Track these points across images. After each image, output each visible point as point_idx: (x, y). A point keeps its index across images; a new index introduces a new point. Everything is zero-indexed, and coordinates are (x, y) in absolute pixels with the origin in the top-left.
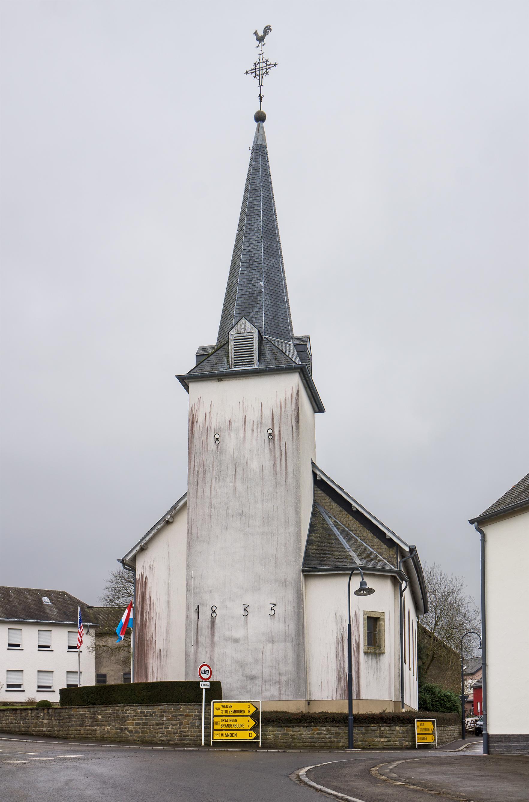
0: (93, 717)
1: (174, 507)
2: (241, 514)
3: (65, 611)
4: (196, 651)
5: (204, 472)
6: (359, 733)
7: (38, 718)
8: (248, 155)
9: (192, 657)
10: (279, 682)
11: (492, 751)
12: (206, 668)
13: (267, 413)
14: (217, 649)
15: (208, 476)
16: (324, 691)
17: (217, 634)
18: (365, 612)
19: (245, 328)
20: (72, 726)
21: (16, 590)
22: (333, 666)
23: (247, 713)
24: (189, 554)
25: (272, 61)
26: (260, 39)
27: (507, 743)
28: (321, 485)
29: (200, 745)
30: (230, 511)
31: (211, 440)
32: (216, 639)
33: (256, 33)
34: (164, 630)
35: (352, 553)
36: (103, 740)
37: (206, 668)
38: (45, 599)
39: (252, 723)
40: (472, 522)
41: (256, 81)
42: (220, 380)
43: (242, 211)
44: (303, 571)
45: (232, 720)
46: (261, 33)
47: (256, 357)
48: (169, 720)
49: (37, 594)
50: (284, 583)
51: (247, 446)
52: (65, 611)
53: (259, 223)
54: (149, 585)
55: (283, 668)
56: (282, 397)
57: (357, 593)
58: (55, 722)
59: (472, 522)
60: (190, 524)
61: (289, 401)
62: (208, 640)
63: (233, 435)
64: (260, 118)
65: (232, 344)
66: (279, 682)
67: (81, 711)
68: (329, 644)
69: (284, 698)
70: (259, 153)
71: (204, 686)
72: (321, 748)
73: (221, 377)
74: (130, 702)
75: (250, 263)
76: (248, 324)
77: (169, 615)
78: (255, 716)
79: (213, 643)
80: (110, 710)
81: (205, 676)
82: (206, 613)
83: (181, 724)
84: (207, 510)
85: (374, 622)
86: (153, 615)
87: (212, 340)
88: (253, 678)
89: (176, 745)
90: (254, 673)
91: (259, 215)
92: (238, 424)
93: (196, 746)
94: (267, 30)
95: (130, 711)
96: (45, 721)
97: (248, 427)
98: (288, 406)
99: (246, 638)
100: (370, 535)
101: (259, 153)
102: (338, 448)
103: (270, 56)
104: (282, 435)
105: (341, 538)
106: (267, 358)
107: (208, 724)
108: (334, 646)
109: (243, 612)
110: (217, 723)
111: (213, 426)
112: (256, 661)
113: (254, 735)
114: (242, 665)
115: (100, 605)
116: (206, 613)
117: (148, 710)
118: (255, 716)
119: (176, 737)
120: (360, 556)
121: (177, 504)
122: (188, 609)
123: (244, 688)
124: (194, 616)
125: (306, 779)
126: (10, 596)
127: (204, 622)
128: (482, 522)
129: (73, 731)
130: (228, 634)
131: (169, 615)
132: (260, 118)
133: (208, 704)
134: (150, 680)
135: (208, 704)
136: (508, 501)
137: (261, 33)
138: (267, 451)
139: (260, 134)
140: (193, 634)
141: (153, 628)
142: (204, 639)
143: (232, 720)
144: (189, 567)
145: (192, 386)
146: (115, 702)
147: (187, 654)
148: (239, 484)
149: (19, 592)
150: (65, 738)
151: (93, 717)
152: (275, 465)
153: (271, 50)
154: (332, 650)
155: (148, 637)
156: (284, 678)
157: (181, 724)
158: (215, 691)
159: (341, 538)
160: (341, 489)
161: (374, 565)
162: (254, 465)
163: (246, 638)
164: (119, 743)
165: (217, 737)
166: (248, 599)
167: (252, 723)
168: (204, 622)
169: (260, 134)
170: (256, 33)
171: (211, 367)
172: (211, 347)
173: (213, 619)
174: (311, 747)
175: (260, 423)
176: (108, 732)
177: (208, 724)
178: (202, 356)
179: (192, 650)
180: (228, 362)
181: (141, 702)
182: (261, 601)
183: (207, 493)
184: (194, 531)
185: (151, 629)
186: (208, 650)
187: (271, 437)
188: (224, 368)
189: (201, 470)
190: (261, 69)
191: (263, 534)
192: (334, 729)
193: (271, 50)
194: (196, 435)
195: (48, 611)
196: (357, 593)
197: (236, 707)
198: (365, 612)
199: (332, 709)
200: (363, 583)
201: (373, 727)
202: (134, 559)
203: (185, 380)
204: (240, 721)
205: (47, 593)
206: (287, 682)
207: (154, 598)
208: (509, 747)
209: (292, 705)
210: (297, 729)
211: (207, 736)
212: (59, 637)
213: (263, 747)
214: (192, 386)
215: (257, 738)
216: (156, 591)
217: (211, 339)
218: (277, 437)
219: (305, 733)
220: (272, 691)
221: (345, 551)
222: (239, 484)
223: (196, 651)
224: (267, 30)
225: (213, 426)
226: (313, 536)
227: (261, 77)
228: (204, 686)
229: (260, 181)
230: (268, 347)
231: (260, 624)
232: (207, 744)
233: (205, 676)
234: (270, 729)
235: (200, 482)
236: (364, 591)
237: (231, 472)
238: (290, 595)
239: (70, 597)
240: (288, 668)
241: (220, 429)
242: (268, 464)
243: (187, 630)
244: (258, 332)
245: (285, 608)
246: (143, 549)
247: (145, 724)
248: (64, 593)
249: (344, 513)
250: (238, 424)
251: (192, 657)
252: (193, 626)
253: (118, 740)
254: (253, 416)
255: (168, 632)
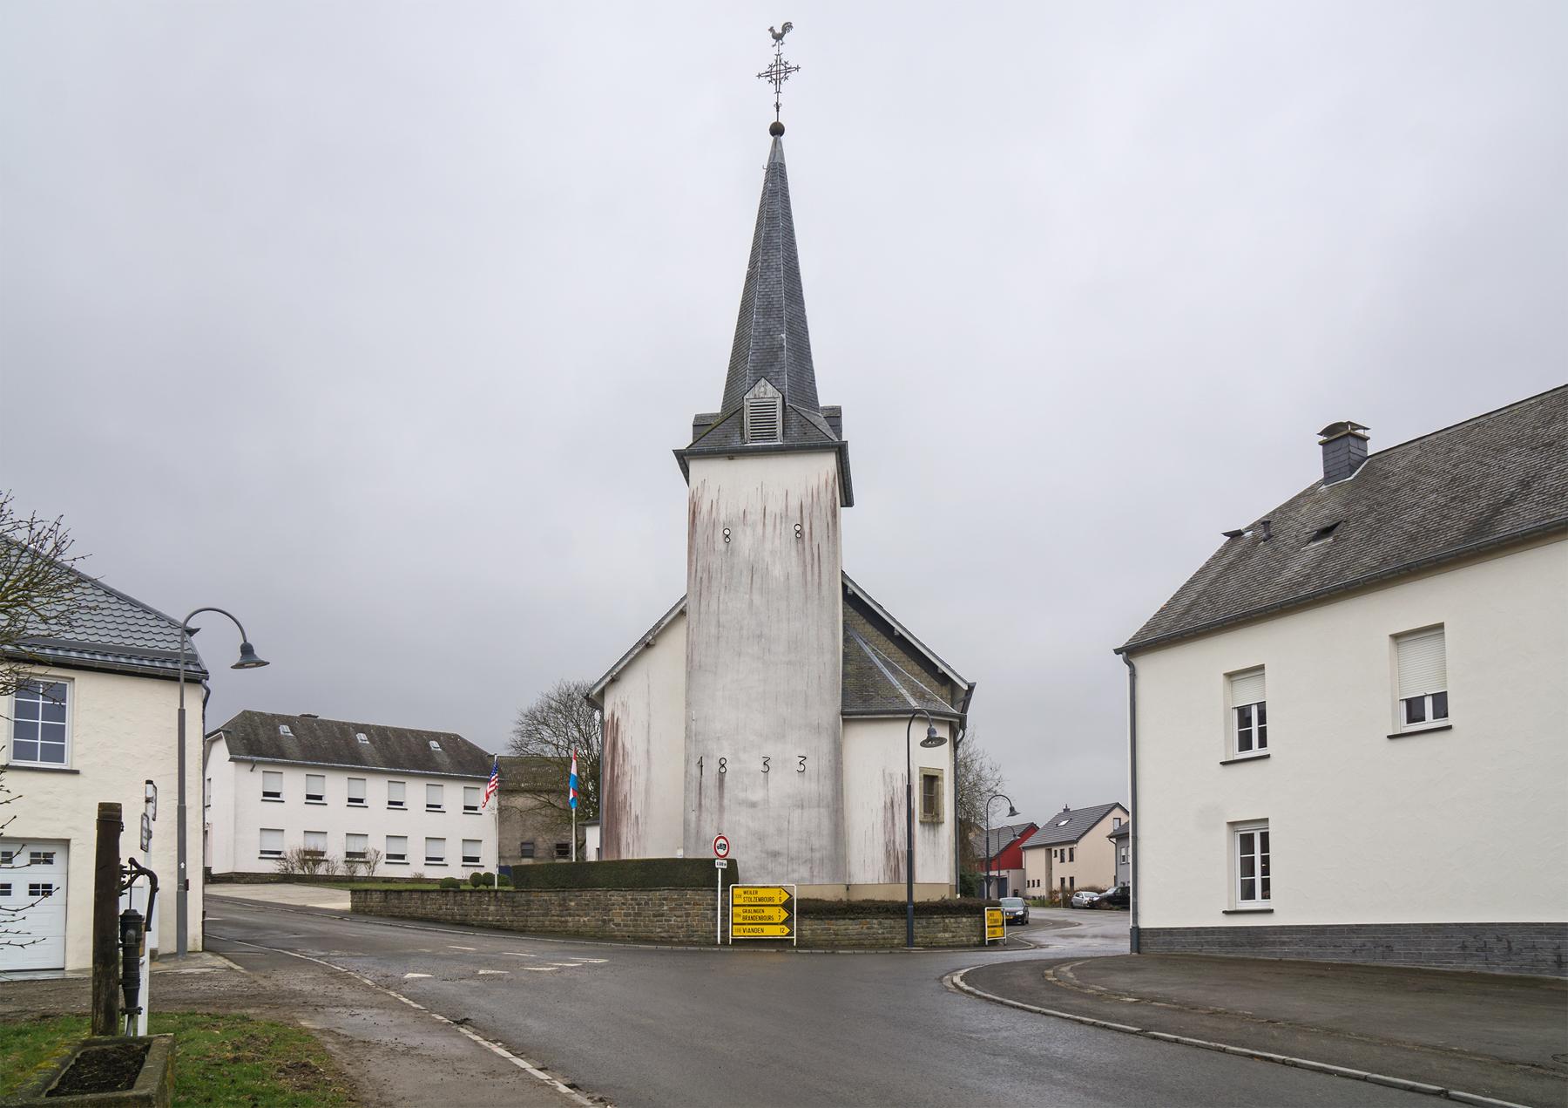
0: (563, 905)
1: (657, 626)
2: (760, 636)
3: (459, 761)
4: (699, 819)
5: (710, 579)
6: (920, 928)
7: (480, 903)
8: (762, 175)
9: (693, 825)
10: (811, 860)
11: (1144, 949)
12: (721, 841)
13: (794, 504)
14: (726, 816)
15: (715, 584)
16: (868, 872)
17: (727, 795)
18: (921, 769)
19: (766, 391)
20: (532, 915)
21: (395, 730)
22: (880, 839)
23: (777, 902)
24: (688, 689)
25: (792, 64)
26: (778, 37)
27: (1168, 938)
28: (854, 602)
29: (715, 944)
30: (745, 632)
31: (720, 537)
32: (726, 802)
33: (771, 29)
34: (642, 788)
35: (904, 691)
36: (577, 935)
37: (721, 841)
38: (434, 744)
39: (785, 915)
40: (1118, 652)
41: (772, 86)
42: (731, 458)
43: (755, 243)
44: (843, 714)
45: (757, 910)
46: (779, 30)
47: (779, 430)
48: (671, 909)
49: (423, 737)
50: (818, 729)
51: (768, 546)
52: (459, 761)
53: (779, 259)
54: (621, 728)
55: (816, 843)
56: (814, 482)
57: (923, 744)
58: (506, 909)
59: (1118, 652)
60: (691, 646)
61: (823, 488)
62: (715, 804)
63: (749, 531)
64: (777, 130)
65: (747, 411)
66: (811, 860)
67: (546, 896)
68: (863, 812)
69: (817, 881)
70: (776, 173)
71: (721, 865)
72: (872, 946)
73: (732, 454)
74: (617, 886)
75: (768, 310)
76: (769, 387)
77: (649, 769)
78: (787, 906)
79: (721, 808)
80: (587, 895)
81: (722, 852)
82: (712, 767)
83: (688, 915)
84: (713, 631)
85: (931, 780)
86: (627, 768)
87: (714, 406)
88: (775, 855)
89: (681, 943)
90: (777, 848)
91: (778, 250)
92: (754, 516)
93: (708, 945)
94: (787, 27)
95: (616, 897)
96: (492, 908)
97: (769, 521)
98: (822, 495)
99: (766, 801)
100: (917, 668)
101: (776, 173)
102: (880, 551)
103: (790, 57)
104: (813, 534)
105: (886, 671)
106: (794, 431)
107: (725, 916)
108: (881, 814)
109: (761, 767)
110: (737, 914)
111: (722, 517)
112: (780, 831)
113: (787, 930)
114: (761, 837)
115: (505, 753)
116: (712, 767)
117: (643, 896)
118: (787, 906)
119: (681, 933)
120: (913, 695)
121: (660, 622)
122: (687, 761)
123: (763, 867)
124: (695, 770)
125: (962, 984)
126: (388, 739)
127: (708, 779)
128: (1131, 652)
129: (532, 922)
130: (742, 795)
131: (649, 769)
132: (777, 130)
133: (725, 890)
134: (624, 857)
135: (725, 890)
136: (1166, 625)
137: (779, 30)
138: (794, 553)
139: (777, 150)
140: (694, 796)
141: (626, 787)
142: (710, 801)
143: (757, 910)
144: (688, 704)
145: (694, 466)
146: (594, 885)
147: (686, 823)
148: (757, 598)
149: (400, 733)
150: (522, 931)
151: (563, 905)
152: (804, 573)
153: (791, 50)
154: (878, 818)
155: (621, 798)
156: (817, 855)
157: (688, 915)
158: (732, 874)
159: (886, 671)
160: (880, 606)
161: (932, 707)
162: (777, 571)
163: (766, 801)
164: (601, 939)
165: (737, 932)
166: (769, 749)
167: (785, 915)
168: (708, 779)
169: (777, 150)
170: (771, 29)
171: (714, 440)
172: (712, 416)
173: (722, 776)
174: (860, 946)
175: (785, 516)
176: (585, 925)
177: (725, 916)
178: (702, 425)
179: (693, 817)
180: (742, 435)
181: (632, 886)
182: (787, 752)
183: (714, 606)
184: (696, 658)
185: (624, 788)
186: (715, 817)
187: (800, 534)
188: (736, 443)
189: (705, 576)
190: (778, 73)
191: (789, 663)
192: (888, 921)
193: (791, 50)
194: (699, 529)
195: (439, 759)
196: (923, 744)
197: (762, 893)
198: (921, 769)
199: (879, 895)
200: (930, 732)
201: (936, 919)
202: (602, 693)
203: (683, 458)
204: (768, 911)
205: (435, 736)
206: (822, 860)
207: (628, 746)
208: (1171, 943)
209: (829, 892)
210: (841, 922)
211: (725, 931)
212: (453, 795)
213: (799, 946)
214: (694, 466)
215: (791, 934)
216: (631, 737)
217: (714, 405)
218: (807, 536)
219: (850, 928)
220: (803, 872)
221: (893, 688)
222: (757, 598)
223: (699, 819)
224: (787, 27)
225: (722, 517)
226: (849, 668)
227: (778, 82)
228: (721, 865)
229: (778, 207)
230: (794, 416)
231: (784, 782)
232: (725, 942)
233: (722, 852)
234: (807, 922)
235: (704, 593)
236: (931, 741)
237: (746, 579)
238: (825, 745)
239: (465, 742)
240: (823, 842)
241: (731, 522)
242: (795, 570)
243: (686, 789)
244: (771, 400)
245: (819, 762)
246: (614, 681)
247: (638, 914)
248: (457, 736)
249: (883, 638)
250: (754, 516)
251: (693, 825)
252: (695, 785)
253: (599, 937)
254: (775, 507)
255: (647, 791)
